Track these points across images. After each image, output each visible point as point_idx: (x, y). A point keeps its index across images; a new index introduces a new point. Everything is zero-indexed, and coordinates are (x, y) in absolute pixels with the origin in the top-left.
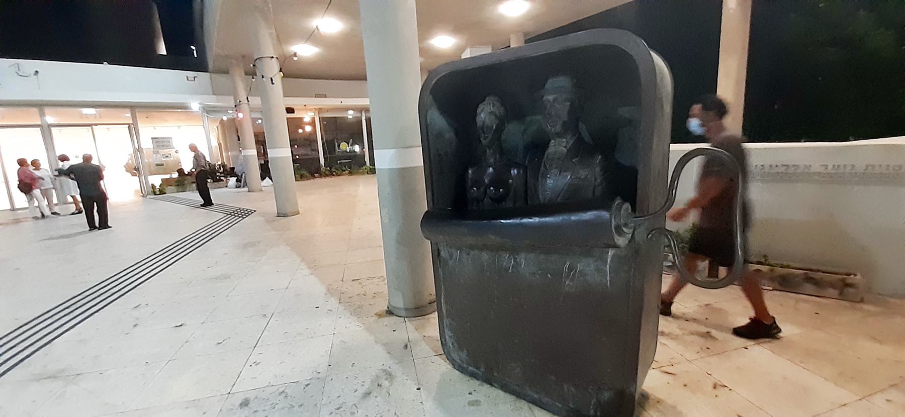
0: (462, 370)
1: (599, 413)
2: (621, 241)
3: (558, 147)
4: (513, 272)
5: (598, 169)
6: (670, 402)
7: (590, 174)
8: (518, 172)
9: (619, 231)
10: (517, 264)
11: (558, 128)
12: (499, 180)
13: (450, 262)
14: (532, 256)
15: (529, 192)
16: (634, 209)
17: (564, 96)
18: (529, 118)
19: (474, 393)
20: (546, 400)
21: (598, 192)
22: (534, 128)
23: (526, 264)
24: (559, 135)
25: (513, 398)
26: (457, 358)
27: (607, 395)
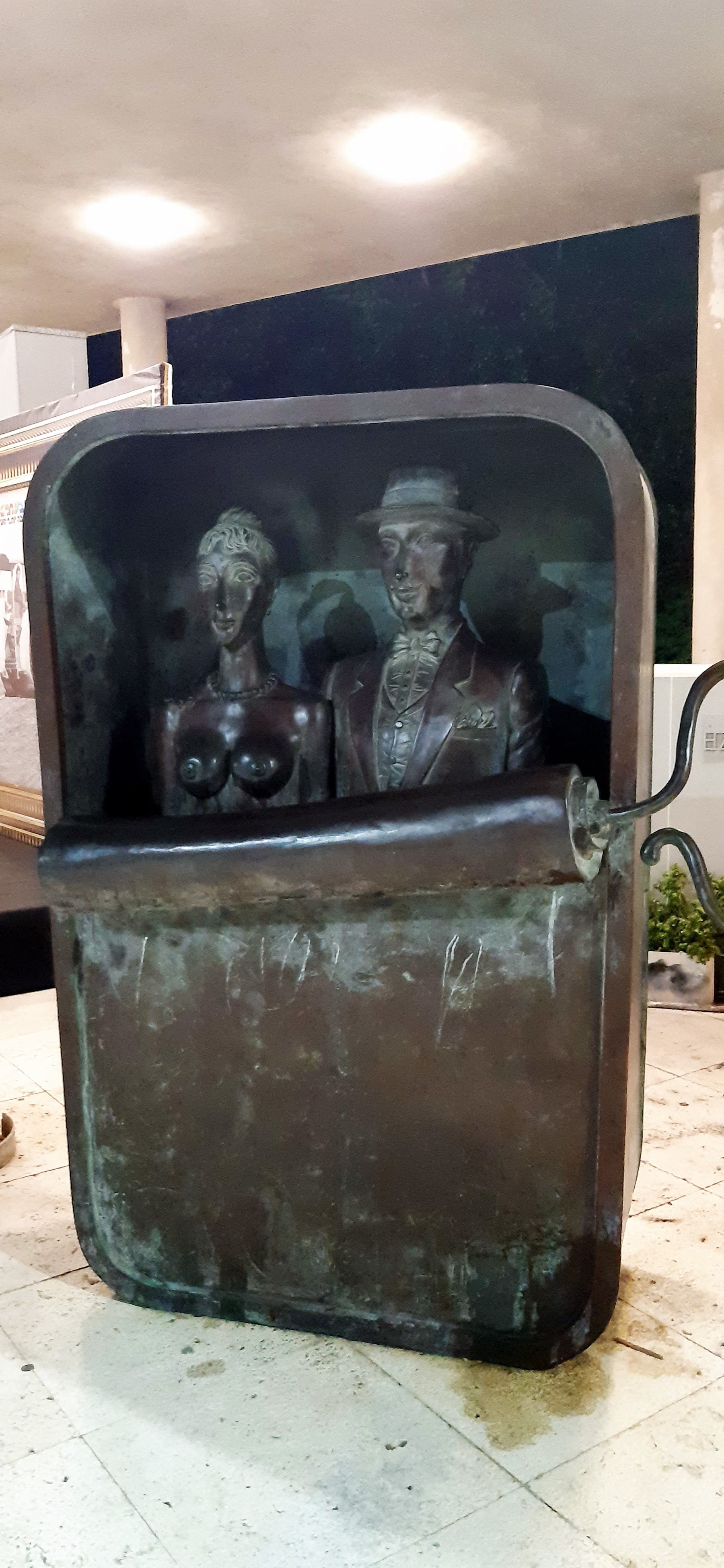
0: (146, 1296)
1: (534, 1317)
2: (587, 866)
3: (417, 650)
4: (308, 979)
5: (515, 707)
6: (676, 1277)
7: (494, 714)
8: (312, 718)
9: (584, 846)
10: (320, 956)
11: (420, 605)
12: (261, 736)
13: (116, 975)
14: (360, 930)
15: (341, 767)
16: (604, 794)
17: (435, 527)
18: (316, 577)
19: (197, 1348)
20: (398, 1319)
21: (517, 758)
22: (331, 602)
23: (347, 951)
24: (419, 622)
25: (310, 1337)
26: (127, 1266)
27: (551, 1263)
